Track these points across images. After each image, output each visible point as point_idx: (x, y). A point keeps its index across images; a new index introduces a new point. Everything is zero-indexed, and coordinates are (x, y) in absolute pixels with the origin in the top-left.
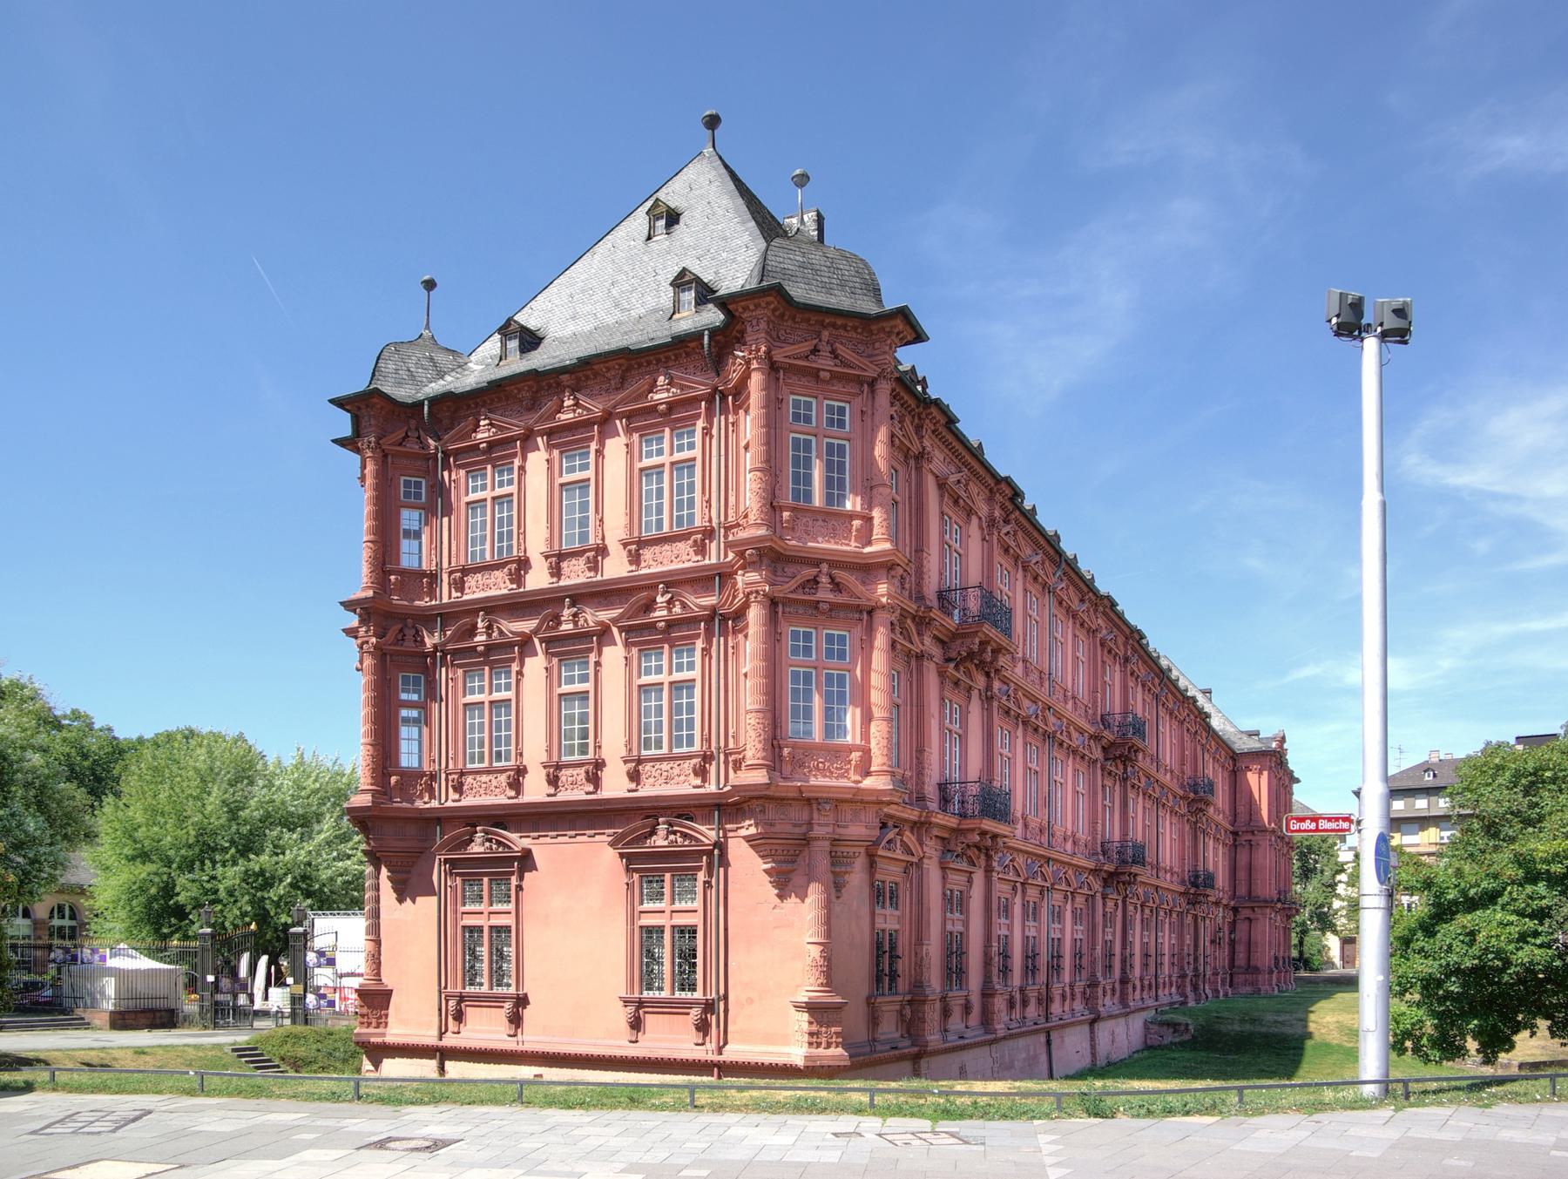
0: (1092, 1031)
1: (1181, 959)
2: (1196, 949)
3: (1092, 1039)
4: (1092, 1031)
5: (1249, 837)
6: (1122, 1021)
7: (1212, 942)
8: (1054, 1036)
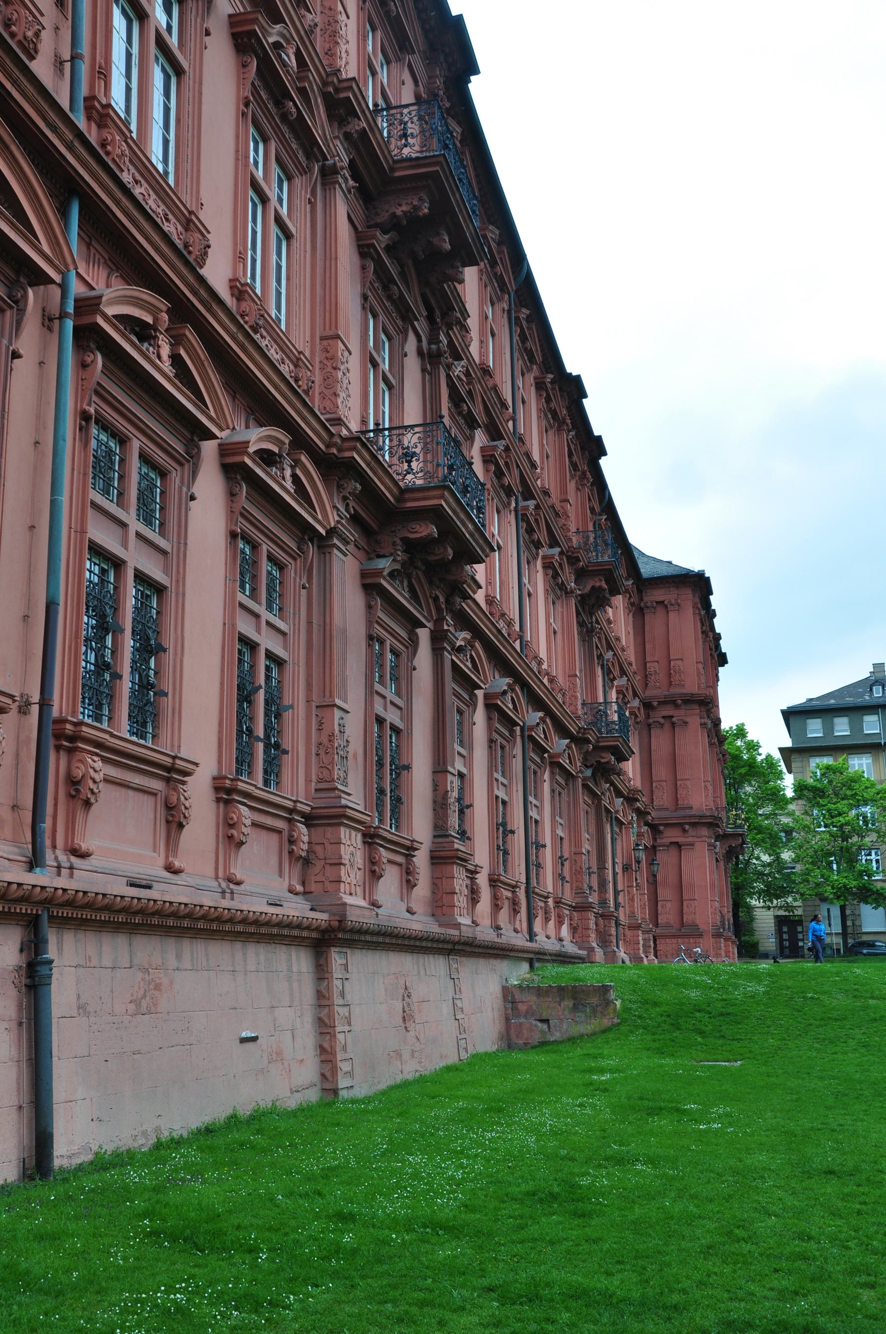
0: (321, 972)
1: (577, 873)
2: (602, 868)
3: (323, 999)
4: (321, 972)
5: (668, 711)
6: (437, 965)
7: (626, 868)
8: (65, 951)
